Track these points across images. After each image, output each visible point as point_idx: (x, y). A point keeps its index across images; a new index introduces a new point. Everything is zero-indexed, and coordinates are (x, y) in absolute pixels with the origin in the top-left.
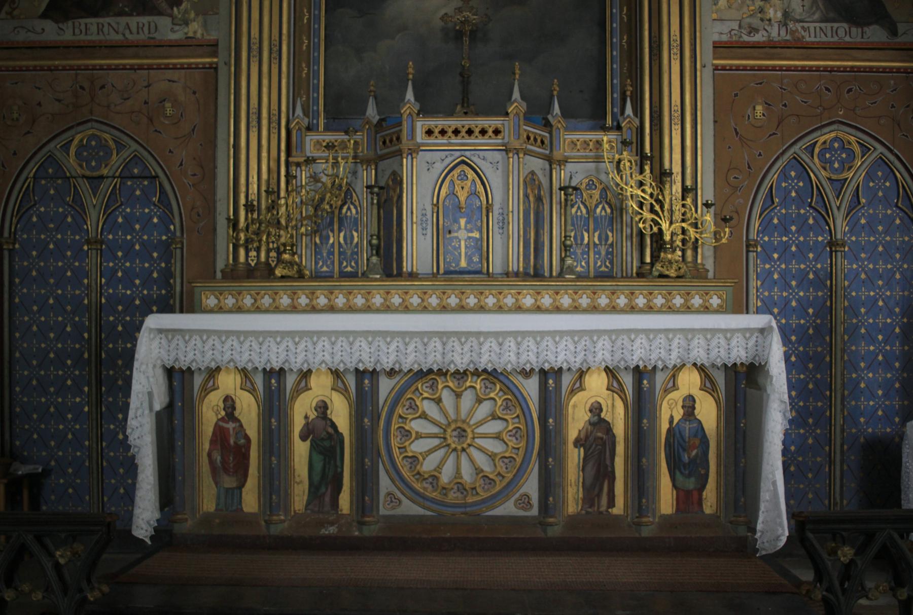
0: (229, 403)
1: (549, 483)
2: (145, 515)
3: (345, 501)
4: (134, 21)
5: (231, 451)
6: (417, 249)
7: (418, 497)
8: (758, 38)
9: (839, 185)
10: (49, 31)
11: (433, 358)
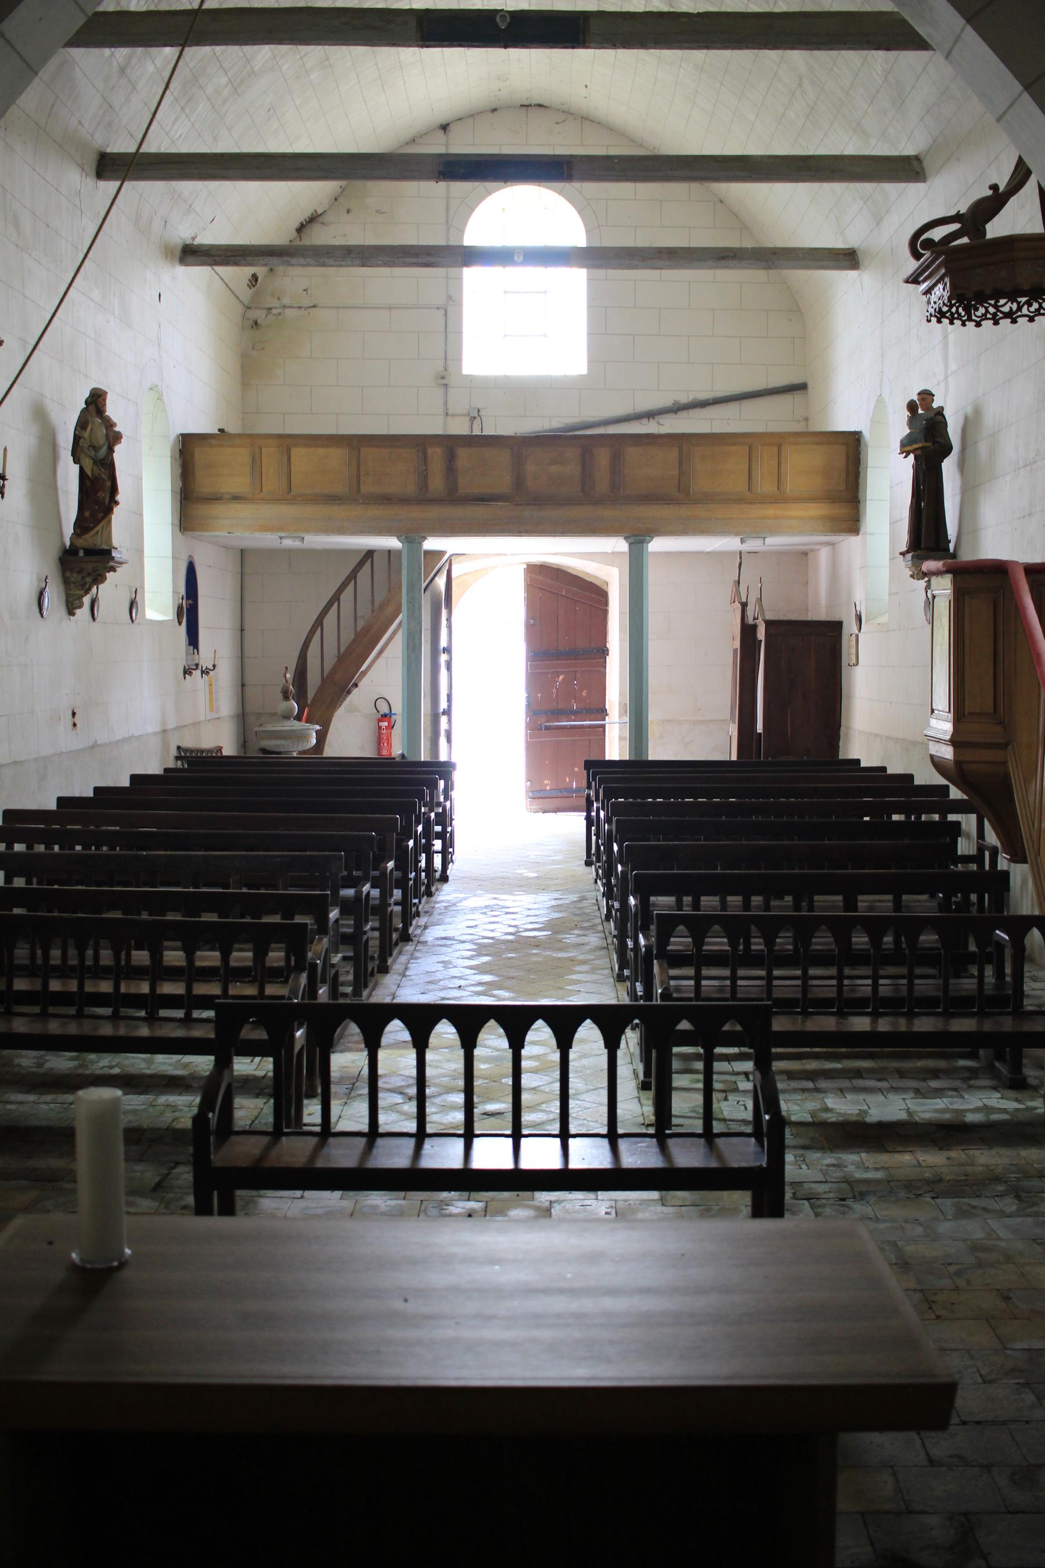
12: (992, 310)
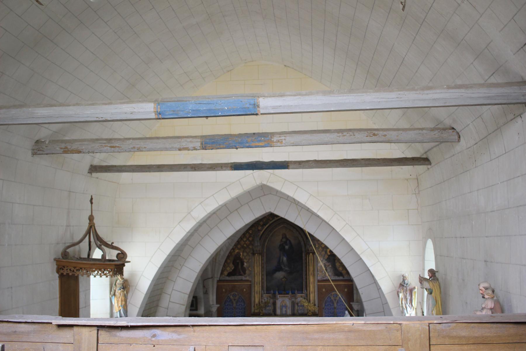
6: (278, 312)
9: (335, 300)
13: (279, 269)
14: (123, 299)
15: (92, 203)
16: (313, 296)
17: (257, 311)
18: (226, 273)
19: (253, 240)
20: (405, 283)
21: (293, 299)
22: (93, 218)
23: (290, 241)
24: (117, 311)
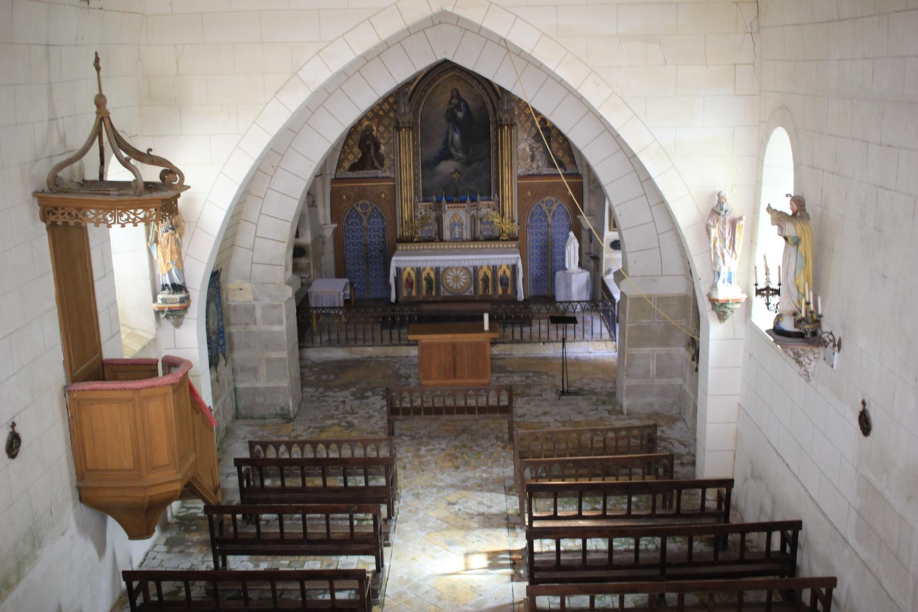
0: (409, 274)
1: (476, 288)
2: (393, 298)
3: (434, 293)
4: (372, 171)
5: (410, 283)
6: (447, 235)
7: (448, 292)
8: (531, 173)
9: (550, 211)
10: (351, 175)
11: (451, 264)
12: (132, 216)
13: (445, 155)
14: (174, 248)
15: (98, 69)
16: (511, 204)
17: (406, 234)
18: (347, 165)
19: (396, 102)
20: (722, 209)
21: (474, 212)
22: (105, 101)
23: (466, 103)
24: (165, 272)
